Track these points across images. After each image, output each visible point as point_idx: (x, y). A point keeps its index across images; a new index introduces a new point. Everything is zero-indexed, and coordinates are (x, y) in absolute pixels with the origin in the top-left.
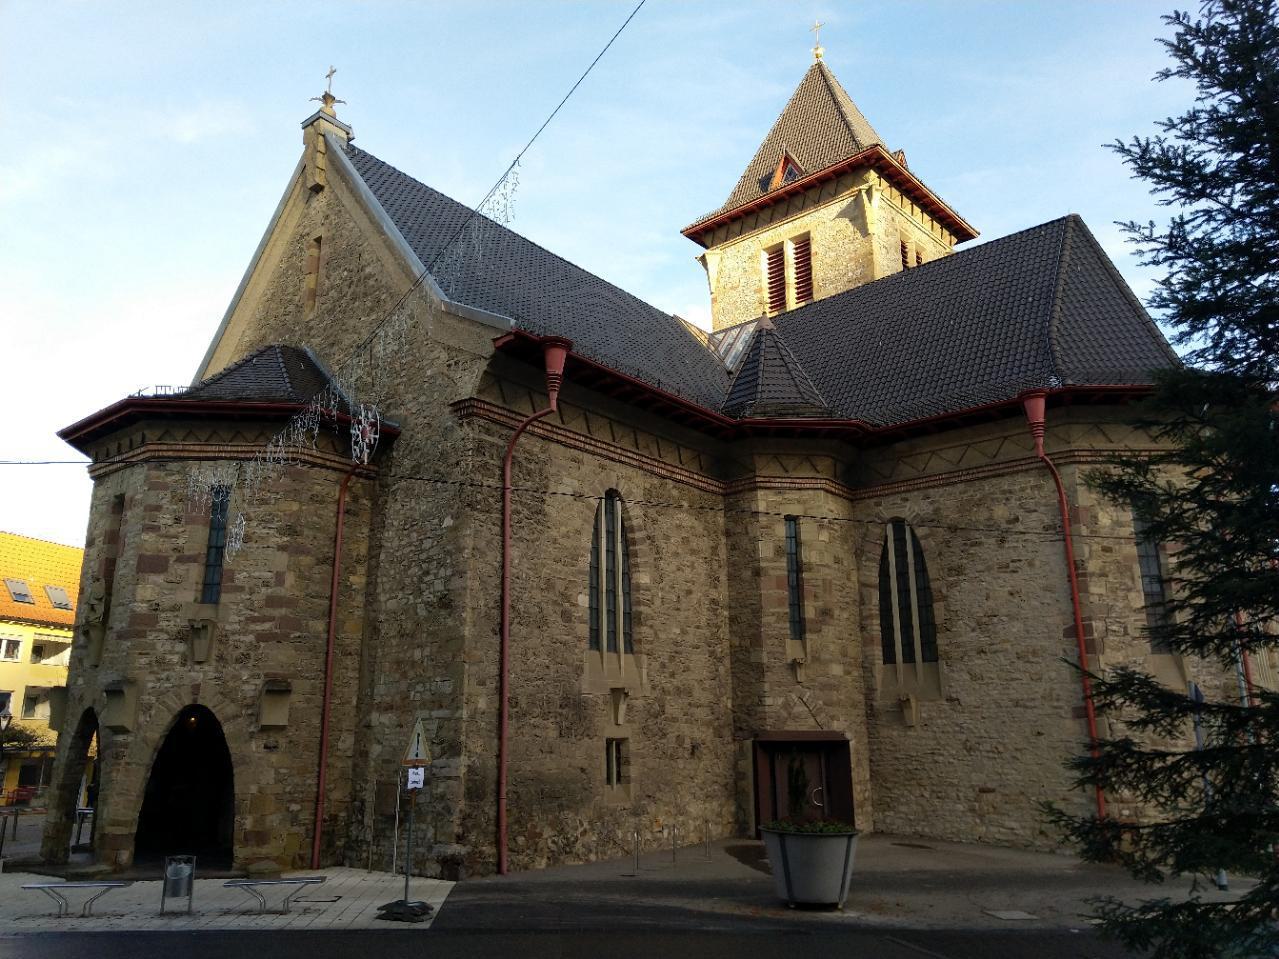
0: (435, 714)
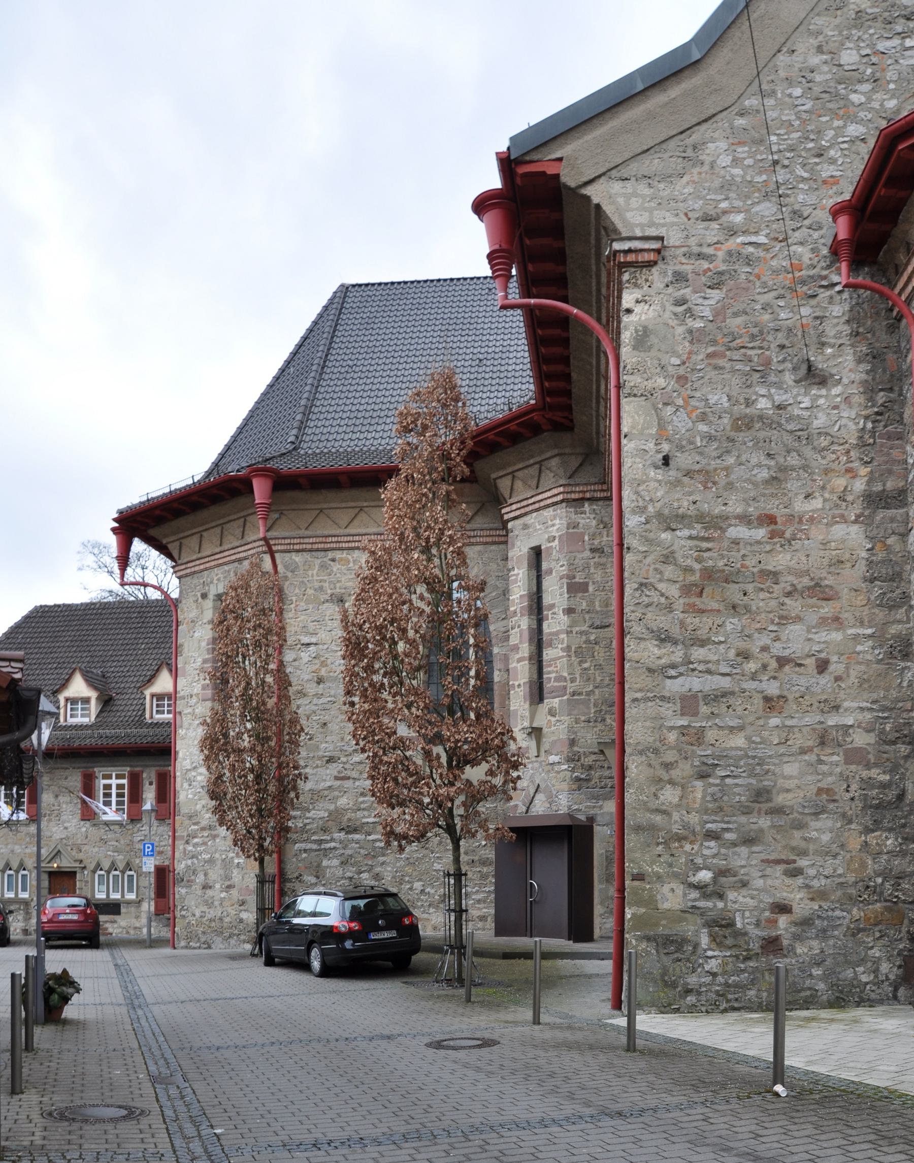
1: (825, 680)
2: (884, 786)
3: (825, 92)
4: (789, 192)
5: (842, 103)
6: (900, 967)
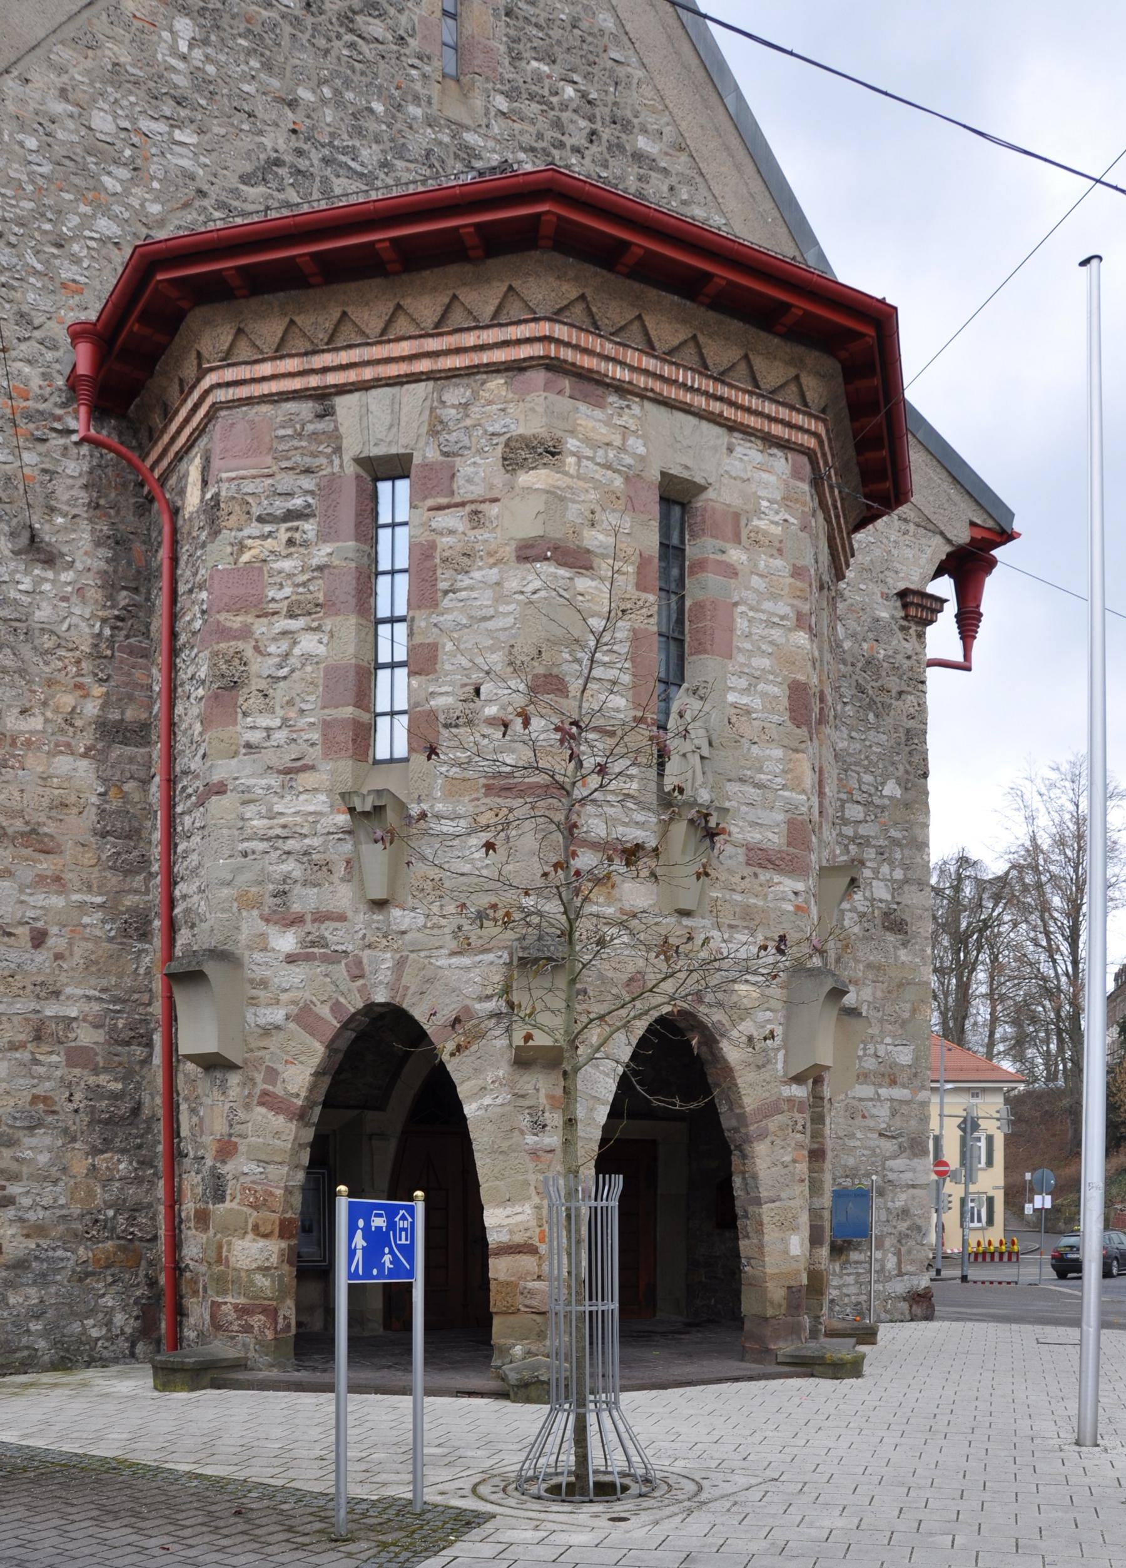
0: (883, 1092)
1: (41, 957)
2: (116, 1097)
3: (68, 157)
4: (16, 283)
5: (91, 183)
6: (137, 1318)
